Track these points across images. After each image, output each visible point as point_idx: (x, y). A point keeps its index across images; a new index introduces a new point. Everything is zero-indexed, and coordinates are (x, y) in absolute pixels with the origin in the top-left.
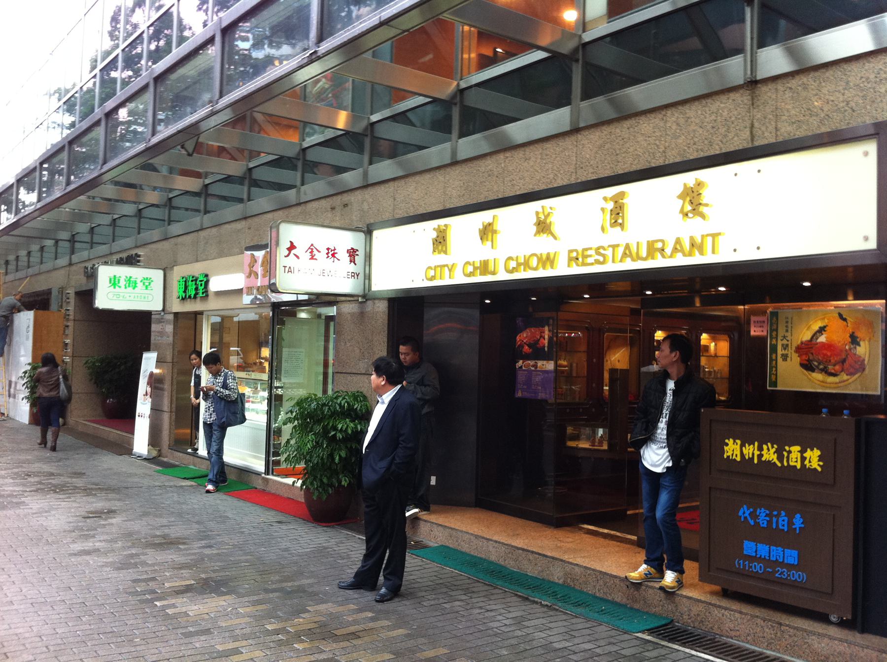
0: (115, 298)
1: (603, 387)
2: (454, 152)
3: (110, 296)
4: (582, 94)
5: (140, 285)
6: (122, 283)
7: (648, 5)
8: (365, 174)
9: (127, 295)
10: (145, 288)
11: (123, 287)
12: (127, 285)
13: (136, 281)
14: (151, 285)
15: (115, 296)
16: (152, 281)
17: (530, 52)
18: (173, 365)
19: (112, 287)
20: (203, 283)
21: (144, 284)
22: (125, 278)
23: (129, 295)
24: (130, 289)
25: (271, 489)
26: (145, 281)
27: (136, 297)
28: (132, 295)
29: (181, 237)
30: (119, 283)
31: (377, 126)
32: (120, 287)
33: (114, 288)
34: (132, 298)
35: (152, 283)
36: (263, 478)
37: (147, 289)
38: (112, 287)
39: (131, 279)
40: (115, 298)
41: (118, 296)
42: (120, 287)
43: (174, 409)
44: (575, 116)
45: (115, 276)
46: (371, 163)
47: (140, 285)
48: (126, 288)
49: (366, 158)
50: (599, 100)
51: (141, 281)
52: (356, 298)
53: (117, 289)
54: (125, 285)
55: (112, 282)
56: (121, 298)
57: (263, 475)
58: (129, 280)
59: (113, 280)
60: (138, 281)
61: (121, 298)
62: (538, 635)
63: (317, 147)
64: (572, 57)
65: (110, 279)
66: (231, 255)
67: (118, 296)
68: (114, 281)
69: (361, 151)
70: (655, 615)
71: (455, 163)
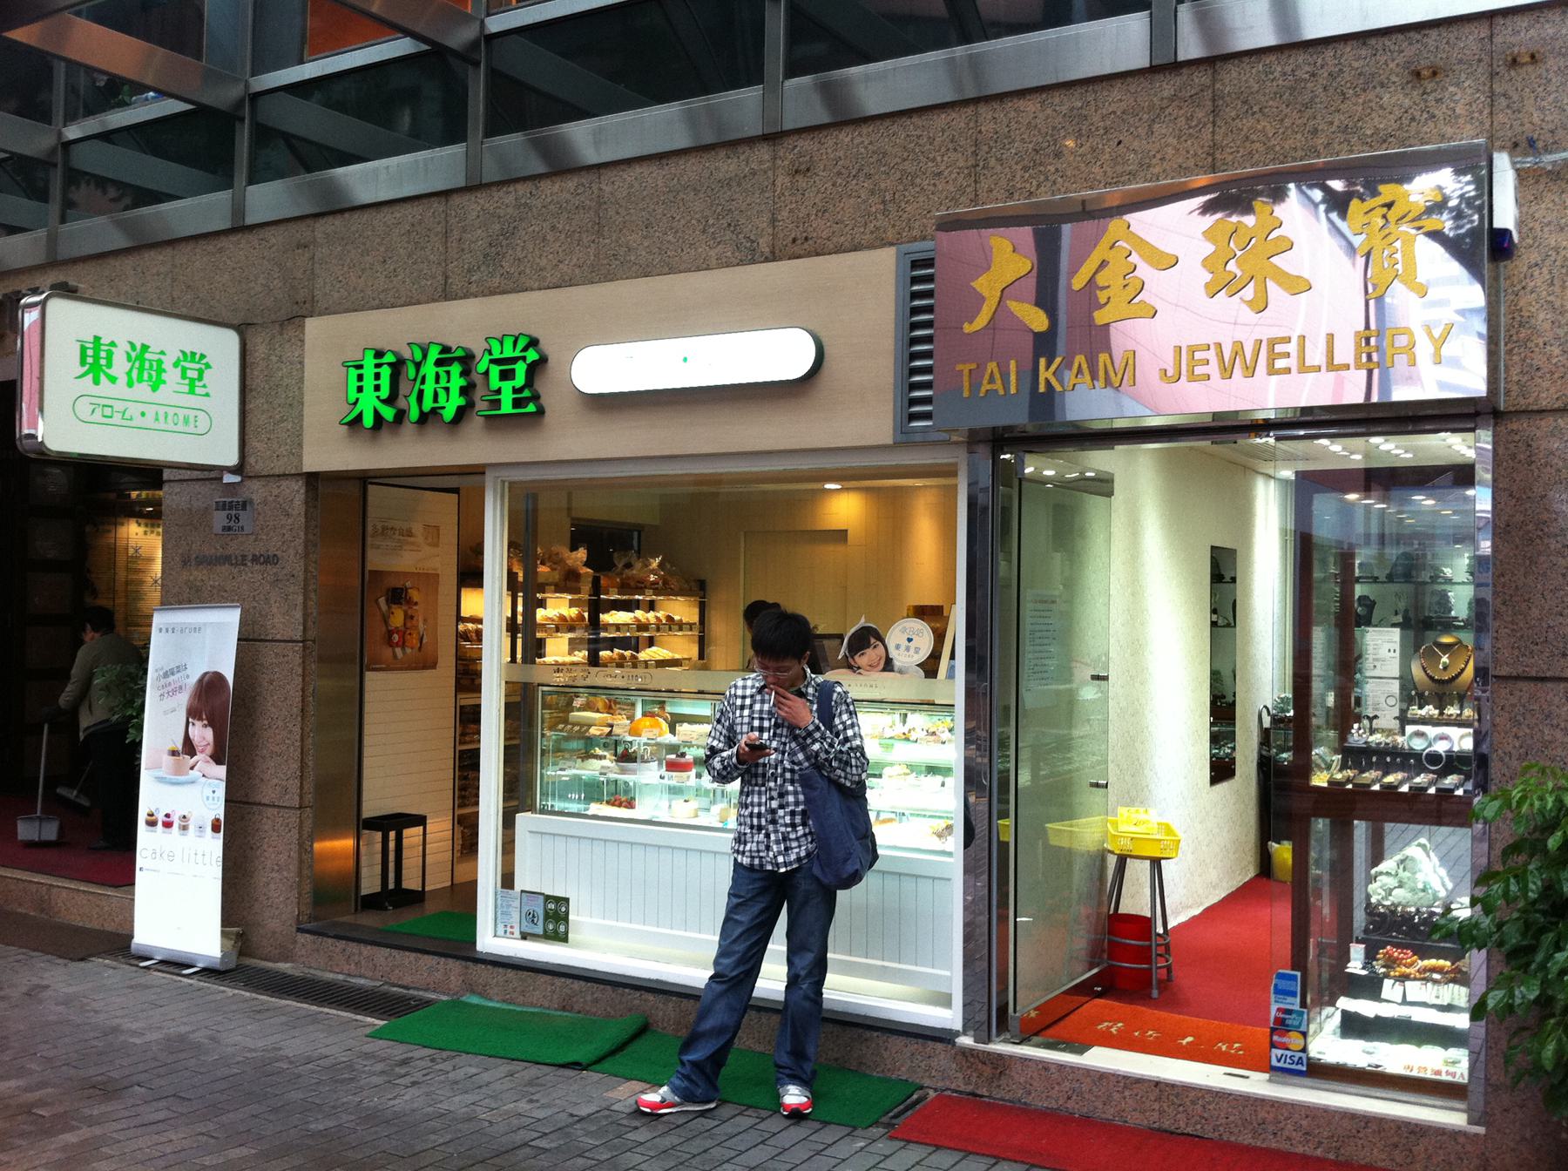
0: (97, 416)
2: (238, 209)
3: (84, 408)
4: (486, 128)
5: (172, 375)
6: (120, 366)
7: (383, 39)
8: (52, 240)
9: (134, 410)
10: (186, 389)
11: (122, 380)
12: (134, 374)
13: (160, 362)
14: (205, 380)
15: (98, 412)
16: (208, 366)
17: (387, 38)
18: (305, 648)
19: (90, 376)
20: (520, 369)
21: (183, 377)
22: (128, 348)
23: (141, 407)
24: (142, 391)
25: (1009, 1090)
26: (187, 365)
27: (161, 418)
28: (150, 411)
29: (385, 209)
30: (109, 365)
31: (75, 149)
32: (113, 380)
33: (96, 382)
34: (149, 421)
35: (207, 373)
36: (966, 1053)
37: (191, 392)
38: (90, 376)
39: (147, 356)
40: (97, 416)
41: (108, 411)
42: (113, 380)
43: (309, 798)
44: (472, 162)
45: (97, 339)
46: (63, 220)
47: (172, 375)
48: (130, 385)
49: (54, 208)
50: (512, 141)
51: (175, 365)
52: (213, 475)
53: (105, 388)
54: (129, 373)
55: (90, 360)
56: (117, 419)
57: (966, 1041)
58: (140, 358)
59: (90, 352)
60: (168, 362)
61: (117, 419)
62: (552, 1141)
63: (282, 93)
64: (468, 56)
65: (83, 349)
66: (672, 270)
67: (108, 411)
68: (96, 357)
69: (42, 196)
71: (240, 228)
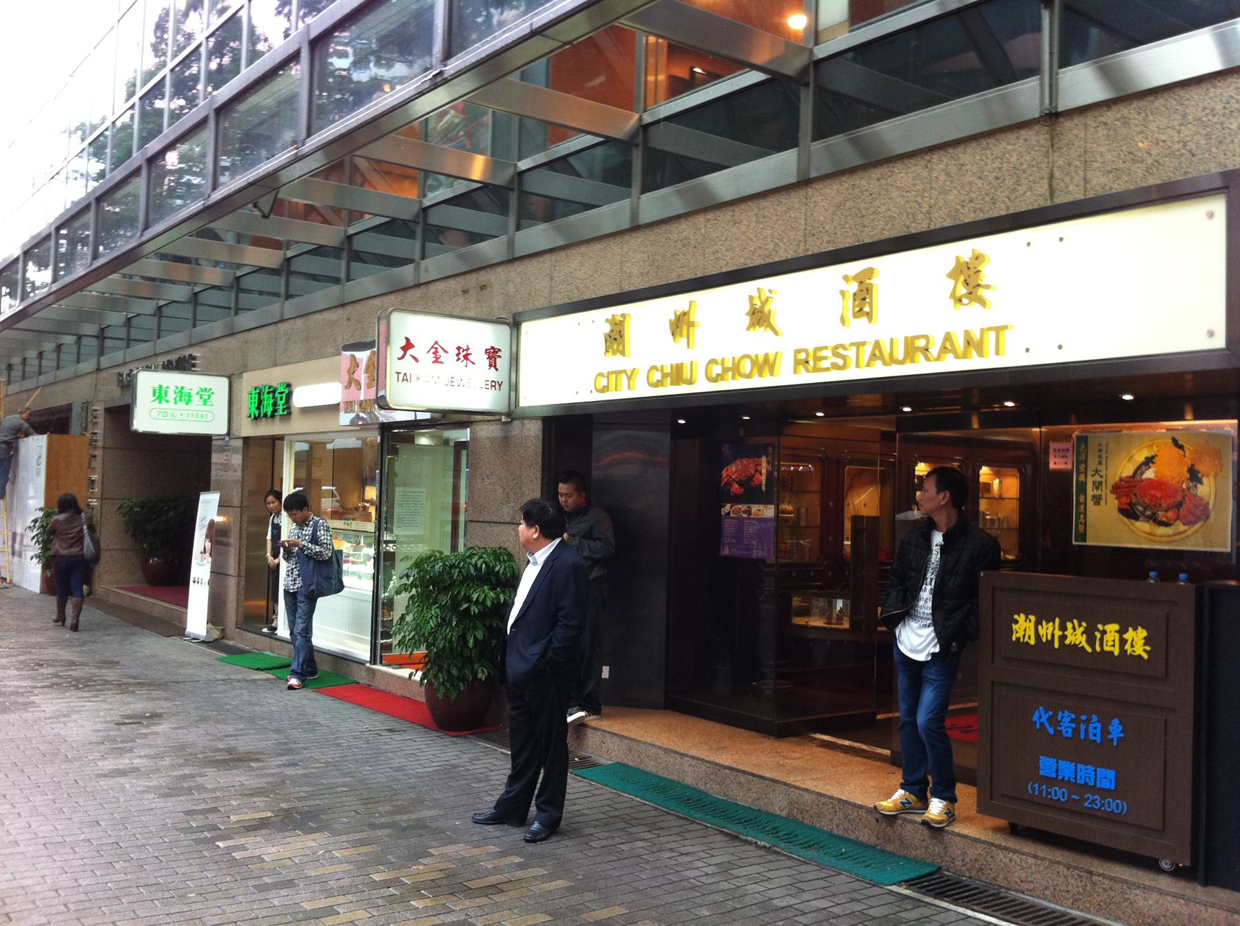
0: (161, 416)
2: (635, 213)
3: (154, 413)
4: (813, 131)
5: (195, 398)
6: (171, 395)
7: (906, 7)
8: (511, 244)
9: (177, 413)
10: (202, 403)
11: (172, 401)
12: (178, 398)
13: (190, 393)
14: (211, 399)
15: (161, 415)
16: (213, 393)
17: (741, 72)
18: (241, 510)
19: (157, 401)
20: (284, 395)
21: (201, 397)
22: (175, 388)
23: (180, 412)
24: (181, 405)
25: (379, 684)
26: (203, 393)
27: (190, 416)
28: (185, 413)
29: (253, 331)
30: (166, 395)
31: (527, 177)
32: (168, 401)
33: (160, 403)
34: (184, 417)
35: (212, 396)
36: (368, 669)
37: (205, 404)
38: (157, 401)
39: (184, 391)
40: (161, 416)
41: (165, 414)
42: (168, 401)
43: (243, 573)
44: (804, 163)
45: (160, 386)
46: (518, 228)
47: (195, 398)
48: (176, 402)
49: (512, 221)
50: (838, 141)
51: (197, 393)
52: (497, 417)
53: (164, 404)
54: (175, 399)
55: (157, 394)
56: (169, 417)
57: (368, 665)
58: (180, 392)
59: (157, 391)
60: (193, 393)
61: (169, 417)
62: (752, 889)
63: (444, 205)
64: (800, 80)
65: (154, 391)
66: (323, 357)
67: (165, 414)
68: (160, 393)
69: (504, 211)
71: (636, 228)
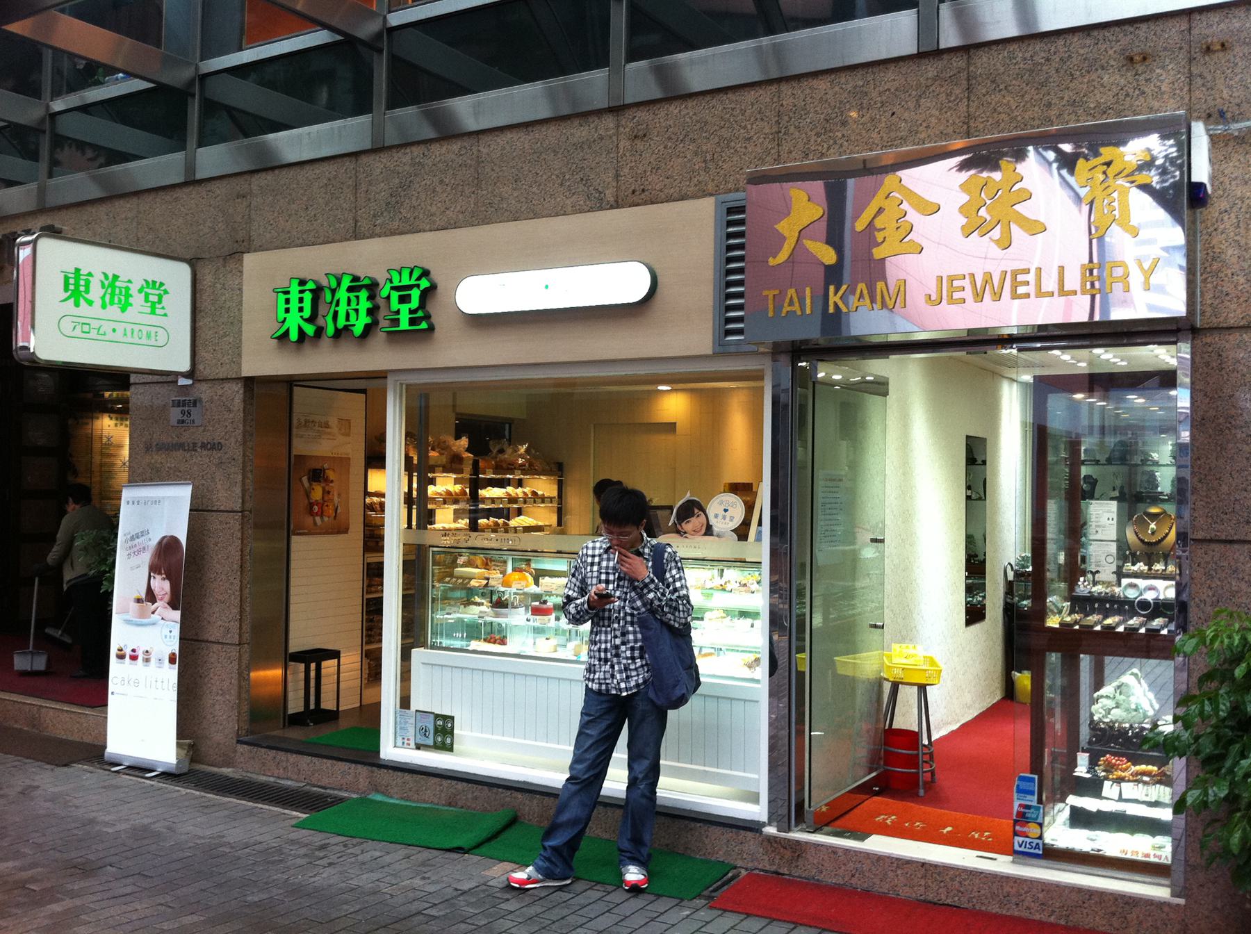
0: (78, 332)
1: (428, 452)
2: (190, 167)
3: (67, 325)
4: (387, 102)
5: (137, 299)
6: (96, 292)
7: (306, 31)
8: (42, 191)
9: (107, 327)
10: (148, 310)
11: (98, 303)
12: (107, 298)
13: (127, 289)
14: (164, 303)
15: (78, 328)
16: (166, 292)
17: (309, 30)
18: (243, 517)
19: (72, 300)
20: (415, 294)
21: (146, 300)
22: (102, 278)
23: (112, 325)
24: (113, 312)
25: (805, 870)
26: (149, 291)
27: (129, 334)
28: (120, 327)
29: (307, 167)
30: (87, 291)
31: (60, 119)
32: (90, 303)
33: (77, 305)
34: (119, 336)
35: (165, 297)
36: (771, 840)
37: (153, 312)
38: (72, 300)
39: (117, 284)
40: (78, 332)
41: (86, 328)
42: (90, 303)
43: (246, 636)
44: (377, 130)
45: (77, 270)
46: (50, 176)
47: (137, 299)
48: (104, 307)
49: (43, 166)
50: (409, 112)
51: (140, 291)
52: (170, 378)
53: (84, 309)
54: (103, 298)
55: (72, 287)
56: (93, 334)
57: (771, 830)
58: (112, 285)
59: (72, 281)
60: (134, 289)
61: (93, 334)
63: (225, 74)
64: (373, 45)
65: (66, 279)
66: (536, 216)
67: (86, 328)
68: (77, 285)
69: (34, 156)
70: (1181, 770)
71: (191, 182)
